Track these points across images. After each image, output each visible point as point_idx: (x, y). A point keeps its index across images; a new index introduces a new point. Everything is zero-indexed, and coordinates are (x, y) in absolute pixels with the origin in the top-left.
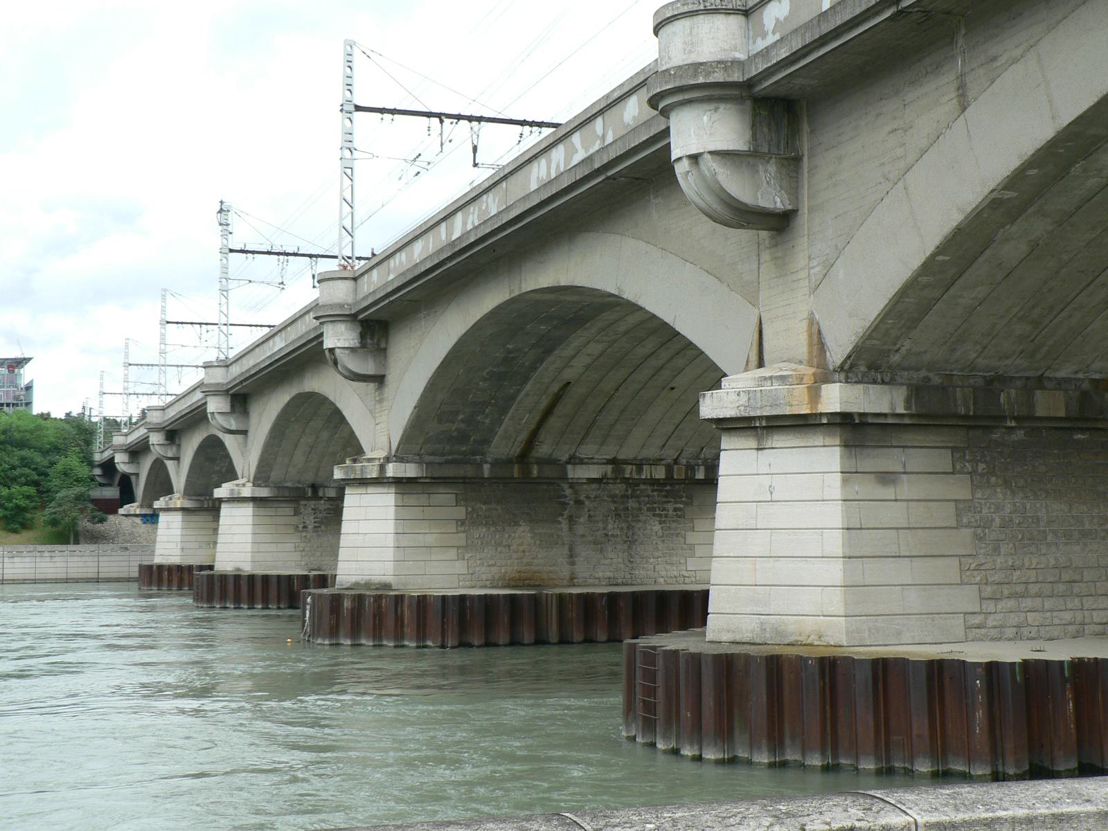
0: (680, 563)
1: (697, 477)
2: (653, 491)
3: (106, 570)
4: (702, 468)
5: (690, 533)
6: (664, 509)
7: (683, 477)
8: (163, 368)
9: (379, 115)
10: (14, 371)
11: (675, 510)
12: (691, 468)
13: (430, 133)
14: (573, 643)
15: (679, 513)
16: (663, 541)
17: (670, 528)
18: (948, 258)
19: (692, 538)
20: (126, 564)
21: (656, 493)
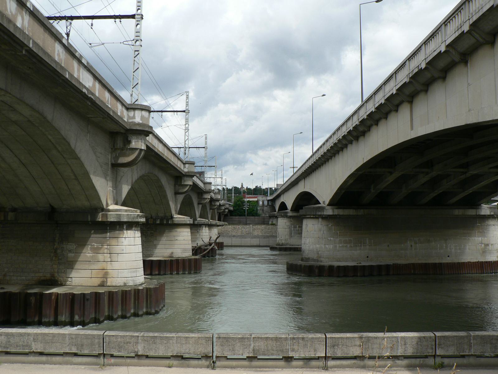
0: (151, 250)
1: (157, 223)
2: (144, 227)
3: (234, 243)
4: (159, 220)
5: (155, 241)
6: (147, 233)
7: (152, 223)
8: (216, 178)
9: (113, 20)
10: (201, 176)
11: (151, 233)
12: (155, 220)
13: (93, 27)
14: (348, 276)
15: (152, 234)
16: (145, 243)
17: (148, 239)
18: (492, 199)
19: (155, 242)
20: (240, 241)
21: (144, 228)
